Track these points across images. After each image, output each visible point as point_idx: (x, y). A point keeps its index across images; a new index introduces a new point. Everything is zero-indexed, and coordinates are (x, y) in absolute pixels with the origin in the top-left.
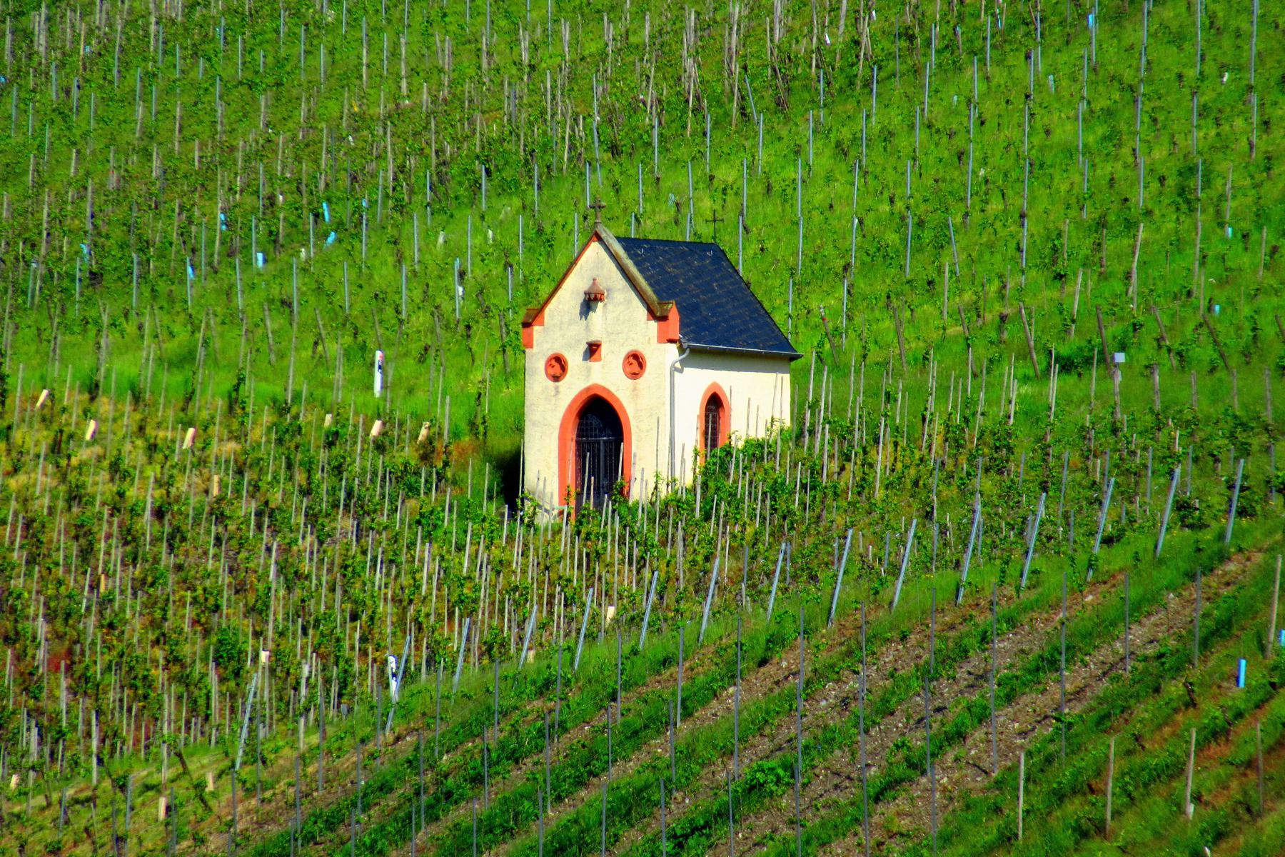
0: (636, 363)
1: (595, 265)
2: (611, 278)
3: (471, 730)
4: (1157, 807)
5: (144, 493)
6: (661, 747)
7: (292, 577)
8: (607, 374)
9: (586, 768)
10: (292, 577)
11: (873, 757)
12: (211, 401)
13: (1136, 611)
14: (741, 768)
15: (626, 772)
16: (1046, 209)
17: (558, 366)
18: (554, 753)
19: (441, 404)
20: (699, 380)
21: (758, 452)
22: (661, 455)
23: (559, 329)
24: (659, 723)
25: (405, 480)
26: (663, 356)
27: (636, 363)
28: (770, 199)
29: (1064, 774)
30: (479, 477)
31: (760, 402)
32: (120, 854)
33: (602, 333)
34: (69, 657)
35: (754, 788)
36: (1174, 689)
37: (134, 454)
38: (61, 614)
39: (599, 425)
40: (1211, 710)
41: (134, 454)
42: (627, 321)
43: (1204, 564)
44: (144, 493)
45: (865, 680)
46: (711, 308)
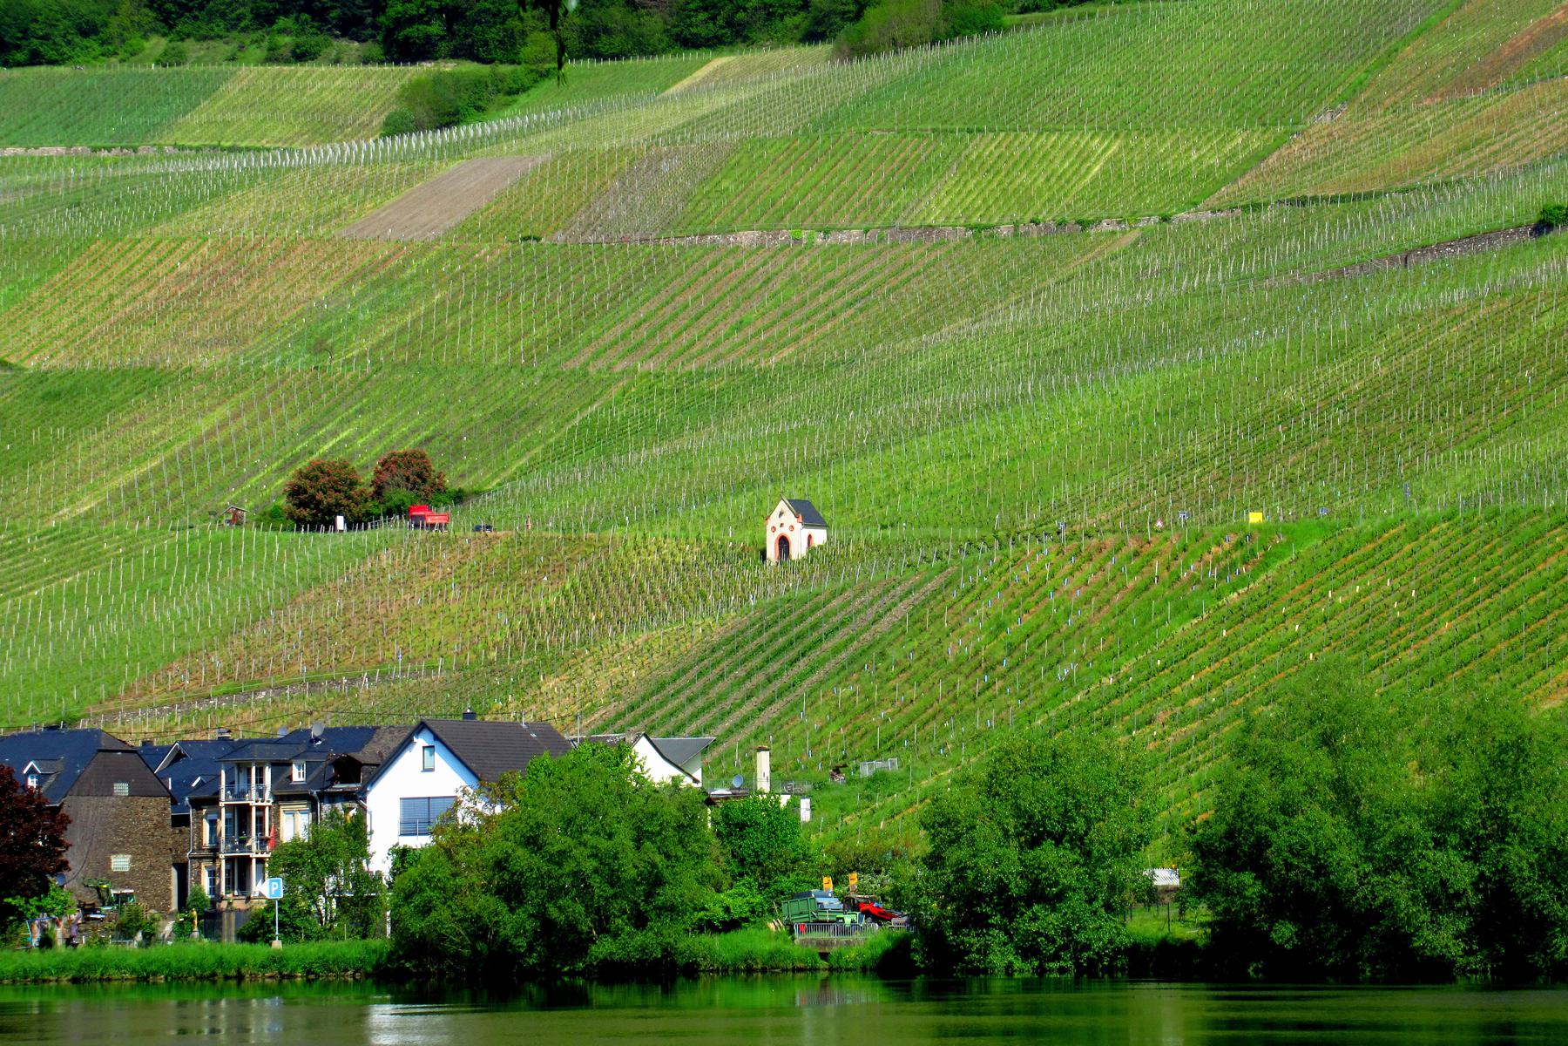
0: (792, 528)
1: (782, 506)
2: (786, 509)
3: (773, 610)
4: (938, 622)
5: (680, 559)
6: (819, 614)
7: (715, 578)
8: (786, 531)
9: (802, 618)
10: (715, 578)
11: (870, 614)
12: (692, 539)
13: (931, 579)
14: (839, 617)
15: (811, 620)
16: (874, 492)
17: (774, 529)
18: (793, 617)
19: (746, 537)
20: (807, 531)
21: (821, 547)
22: (798, 550)
23: (774, 520)
24: (818, 608)
25: (740, 556)
26: (798, 526)
27: (792, 528)
28: (819, 490)
29: (916, 617)
30: (757, 555)
31: (820, 536)
32: (1508, 935)
33: (783, 521)
34: (666, 596)
35: (843, 623)
36: (940, 597)
37: (676, 551)
38: (664, 588)
39: (784, 542)
40: (949, 602)
41: (676, 551)
42: (790, 518)
43: (942, 570)
44: (680, 559)
45: (867, 598)
46: (808, 514)
